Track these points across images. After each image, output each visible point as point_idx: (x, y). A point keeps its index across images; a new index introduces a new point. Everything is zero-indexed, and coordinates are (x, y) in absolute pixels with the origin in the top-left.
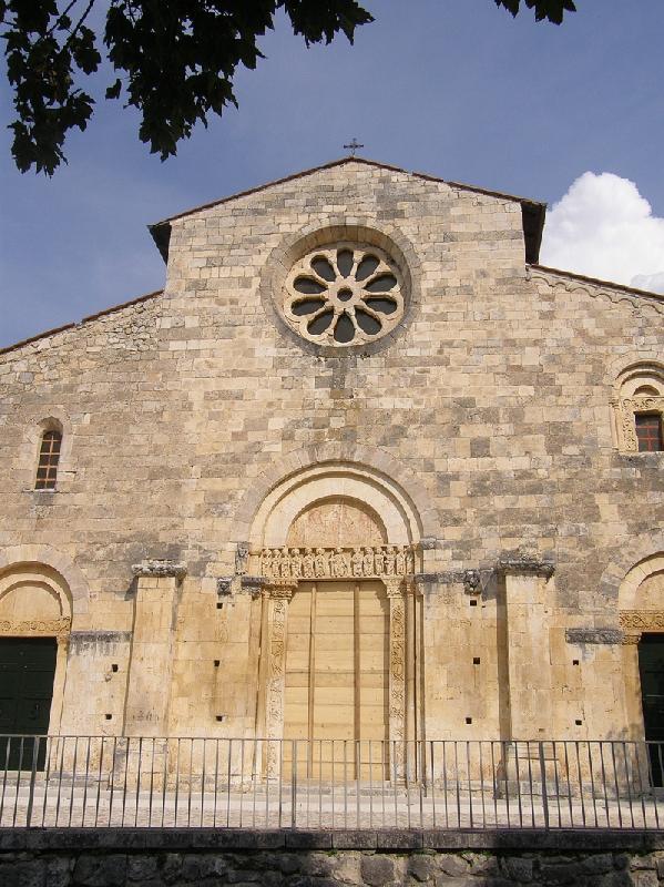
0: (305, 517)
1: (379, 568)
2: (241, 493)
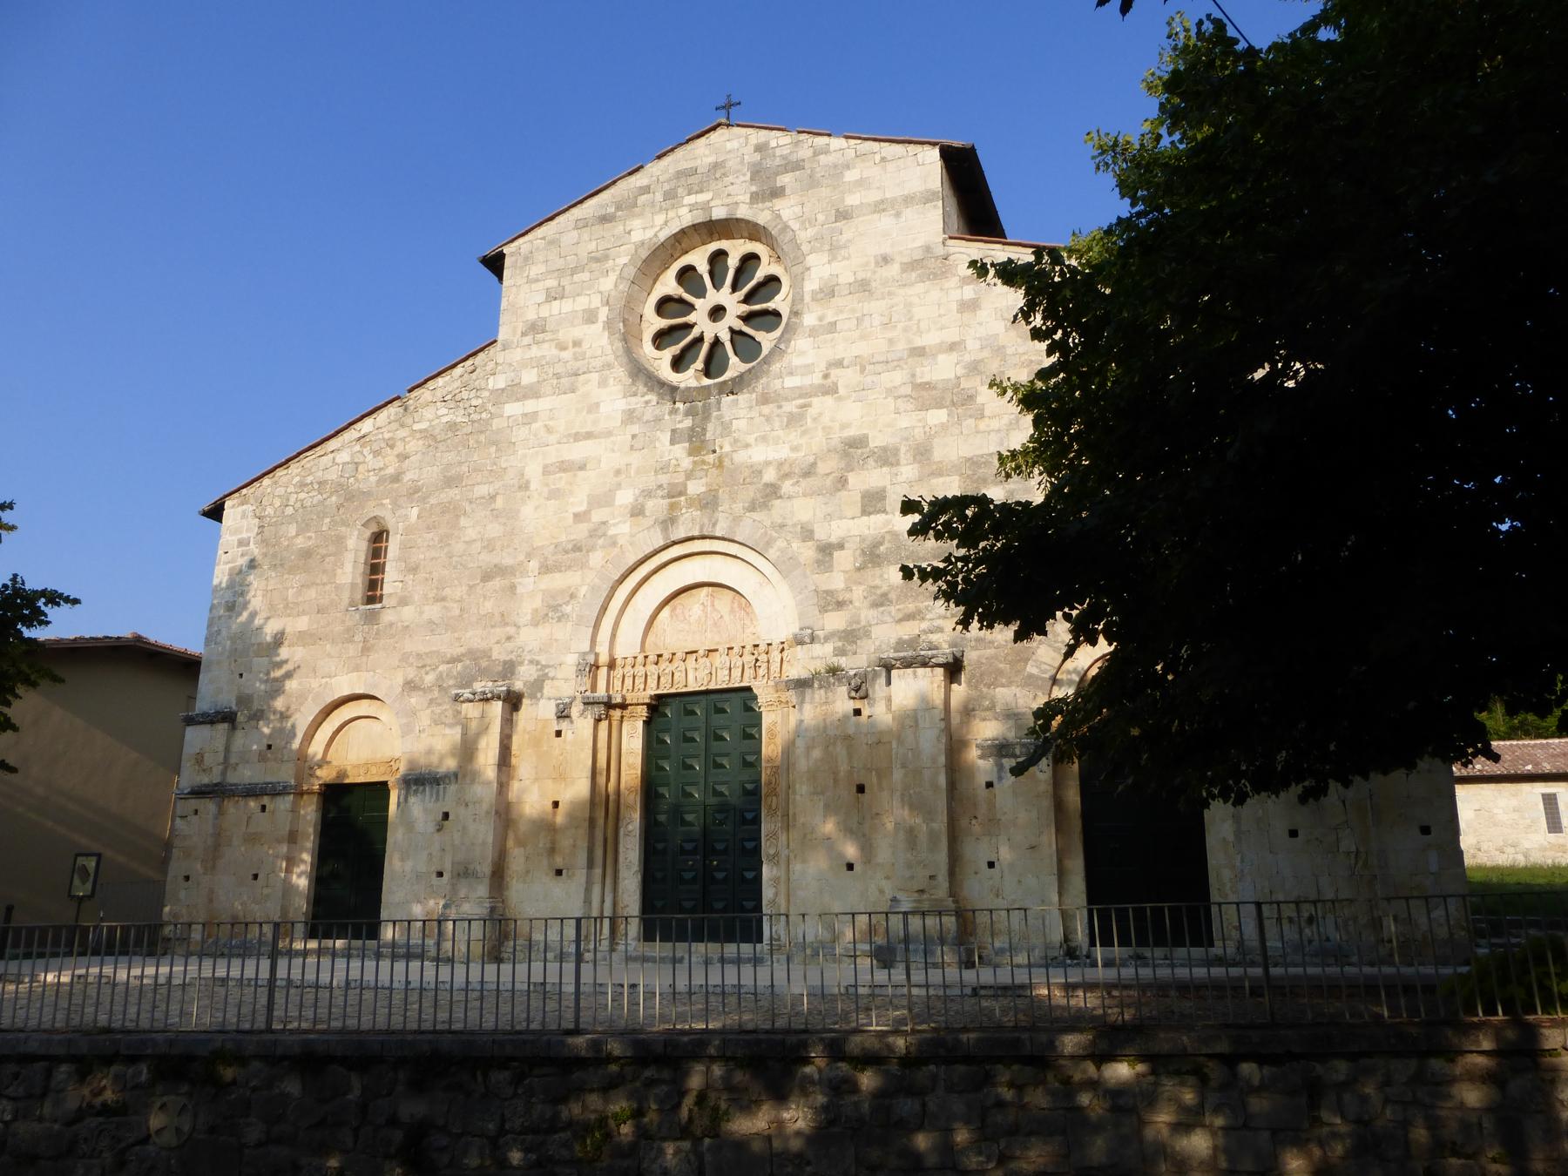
0: (666, 611)
1: (749, 672)
2: (583, 590)
